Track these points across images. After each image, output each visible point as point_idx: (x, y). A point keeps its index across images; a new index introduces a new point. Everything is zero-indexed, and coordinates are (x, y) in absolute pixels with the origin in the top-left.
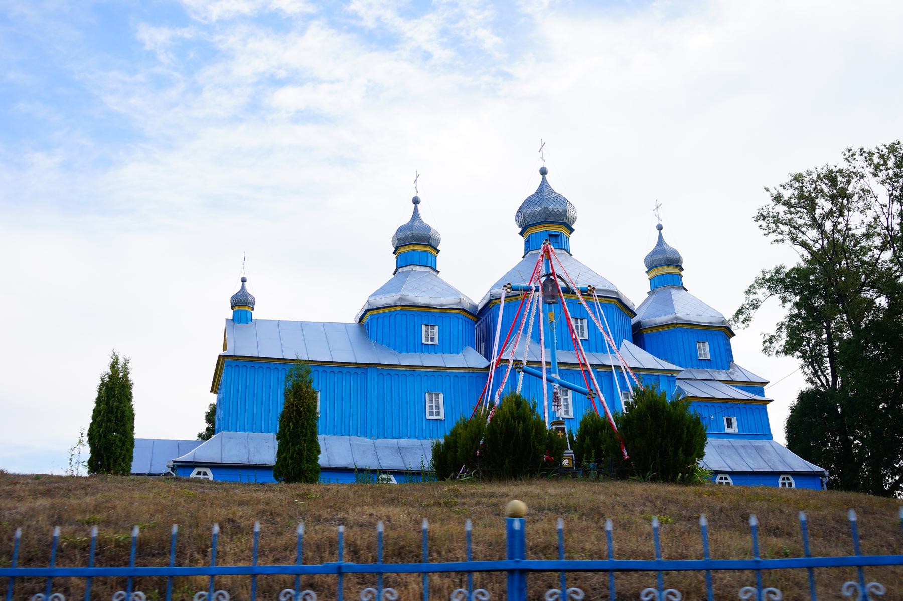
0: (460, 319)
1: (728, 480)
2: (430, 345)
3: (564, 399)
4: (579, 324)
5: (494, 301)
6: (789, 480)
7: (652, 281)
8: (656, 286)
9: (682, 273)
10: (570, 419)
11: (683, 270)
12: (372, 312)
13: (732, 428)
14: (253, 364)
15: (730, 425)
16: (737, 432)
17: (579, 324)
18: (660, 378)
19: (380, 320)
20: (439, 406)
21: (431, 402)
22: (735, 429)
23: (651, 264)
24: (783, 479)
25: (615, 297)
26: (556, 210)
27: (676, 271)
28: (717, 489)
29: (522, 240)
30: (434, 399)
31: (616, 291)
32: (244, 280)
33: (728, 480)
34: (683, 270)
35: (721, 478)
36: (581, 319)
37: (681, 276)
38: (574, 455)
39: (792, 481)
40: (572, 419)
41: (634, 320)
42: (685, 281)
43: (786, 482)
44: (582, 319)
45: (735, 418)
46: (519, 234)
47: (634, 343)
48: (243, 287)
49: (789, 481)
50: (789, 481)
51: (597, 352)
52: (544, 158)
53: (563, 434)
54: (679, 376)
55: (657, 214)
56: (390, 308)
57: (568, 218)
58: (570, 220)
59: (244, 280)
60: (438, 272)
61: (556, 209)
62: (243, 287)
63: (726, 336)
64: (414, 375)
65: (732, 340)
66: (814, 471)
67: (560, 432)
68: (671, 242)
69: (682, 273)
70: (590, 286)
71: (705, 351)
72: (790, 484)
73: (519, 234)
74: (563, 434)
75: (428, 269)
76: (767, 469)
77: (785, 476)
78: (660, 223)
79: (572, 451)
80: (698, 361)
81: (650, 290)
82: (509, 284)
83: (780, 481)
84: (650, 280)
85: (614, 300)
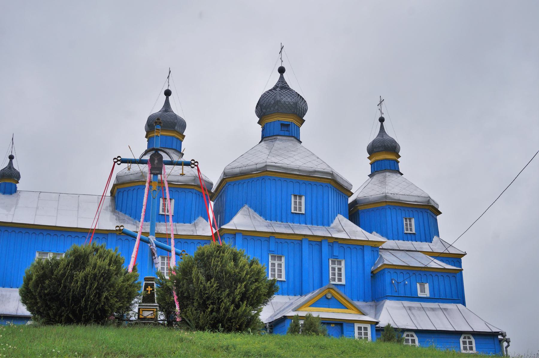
0: (194, 194)
1: (414, 337)
2: (408, 234)
3: (338, 268)
4: (298, 201)
5: (226, 180)
6: (470, 339)
7: (373, 165)
8: (375, 170)
9: (399, 160)
10: (282, 281)
11: (185, 136)
12: (119, 187)
13: (424, 292)
14: (69, 234)
15: (423, 291)
16: (428, 295)
17: (298, 201)
18: (365, 248)
19: (125, 193)
20: (281, 275)
21: (339, 275)
22: (427, 294)
23: (372, 150)
24: (465, 338)
25: (330, 178)
26: (287, 103)
27: (392, 157)
28: (3, 327)
29: (259, 128)
30: (166, 262)
31: (331, 172)
32: (11, 157)
33: (414, 337)
34: (185, 136)
35: (408, 336)
36: (299, 196)
37: (398, 162)
38: (158, 307)
39: (416, 338)
40: (284, 281)
41: (351, 200)
42: (402, 167)
43: (467, 340)
44: (300, 197)
45: (428, 284)
46: (258, 123)
47: (349, 220)
48: (11, 163)
49: (413, 338)
50: (413, 338)
51: (312, 224)
52: (282, 60)
53: (151, 289)
54: (384, 246)
55: (380, 109)
56: (134, 183)
57: (298, 110)
58: (300, 112)
59: (11, 157)
60: (301, 142)
61: (287, 102)
62: (11, 163)
63: (433, 215)
64: (99, 238)
65: (439, 217)
66: (492, 332)
67: (149, 287)
68: (391, 132)
69: (399, 160)
70: (193, 160)
71: (412, 226)
72: (413, 341)
73: (258, 123)
74: (151, 289)
75: (293, 138)
76: (450, 329)
77: (467, 336)
78: (382, 116)
79: (157, 304)
80: (404, 234)
81: (370, 173)
82: (119, 157)
83: (461, 340)
84: (371, 164)
85: (330, 181)
